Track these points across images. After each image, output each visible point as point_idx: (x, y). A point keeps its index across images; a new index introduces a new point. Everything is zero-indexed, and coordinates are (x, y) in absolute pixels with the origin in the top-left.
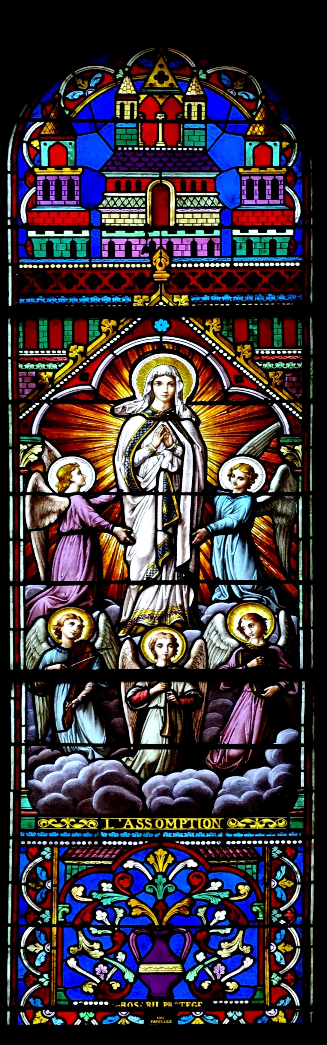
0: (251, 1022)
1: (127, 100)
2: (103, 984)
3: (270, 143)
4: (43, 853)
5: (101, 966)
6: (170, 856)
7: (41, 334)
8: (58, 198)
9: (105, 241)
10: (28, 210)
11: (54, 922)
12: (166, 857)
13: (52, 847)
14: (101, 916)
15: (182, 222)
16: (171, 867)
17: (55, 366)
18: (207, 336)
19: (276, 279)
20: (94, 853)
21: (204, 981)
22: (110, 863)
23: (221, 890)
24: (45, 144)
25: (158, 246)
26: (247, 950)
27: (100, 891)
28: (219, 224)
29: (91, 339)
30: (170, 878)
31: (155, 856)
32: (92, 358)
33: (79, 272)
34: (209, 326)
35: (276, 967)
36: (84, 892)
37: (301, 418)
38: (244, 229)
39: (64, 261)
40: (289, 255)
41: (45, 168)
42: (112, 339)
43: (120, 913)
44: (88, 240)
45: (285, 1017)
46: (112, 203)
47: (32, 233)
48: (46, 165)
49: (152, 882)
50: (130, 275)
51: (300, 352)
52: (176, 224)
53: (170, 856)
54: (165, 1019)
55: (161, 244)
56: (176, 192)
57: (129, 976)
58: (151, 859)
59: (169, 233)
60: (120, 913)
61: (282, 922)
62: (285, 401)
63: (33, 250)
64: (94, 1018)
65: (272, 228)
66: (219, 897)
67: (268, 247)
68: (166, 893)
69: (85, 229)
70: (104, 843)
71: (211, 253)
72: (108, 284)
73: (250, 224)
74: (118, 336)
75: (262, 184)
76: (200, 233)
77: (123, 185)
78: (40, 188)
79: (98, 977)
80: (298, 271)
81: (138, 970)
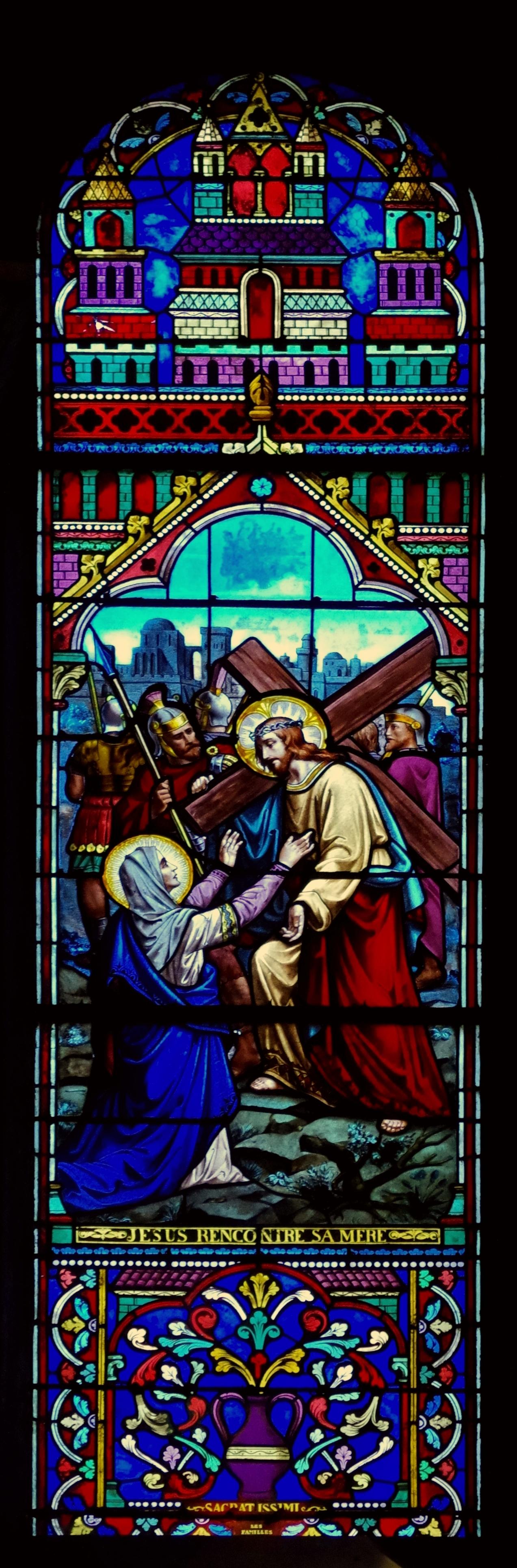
0: (390, 1534)
1: (309, 151)
2: (341, 1476)
3: (422, 214)
4: (83, 1278)
5: (170, 1448)
6: (274, 1283)
7: (437, 500)
8: (411, 295)
9: (179, 361)
10: (66, 311)
11: (101, 1382)
12: (267, 1285)
13: (97, 1269)
14: (169, 1373)
15: (295, 333)
16: (274, 1301)
17: (105, 546)
18: (328, 503)
19: (431, 419)
20: (140, 1278)
21: (321, 1473)
22: (181, 1294)
23: (348, 1336)
24: (90, 214)
25: (256, 369)
26: (384, 1426)
27: (169, 1335)
28: (348, 336)
29: (159, 506)
30: (273, 1317)
31: (251, 1284)
32: (160, 535)
33: (306, 406)
34: (332, 490)
35: (427, 1452)
36: (146, 1337)
37: (466, 629)
38: (384, 345)
39: (117, 390)
40: (449, 384)
41: (90, 249)
42: (189, 506)
43: (199, 1368)
44: (153, 358)
45: (440, 1526)
46: (189, 303)
47: (71, 348)
48: (394, 246)
49: (247, 1323)
50: (451, 413)
51: (464, 531)
52: (283, 336)
53: (274, 1283)
54: (264, 1528)
55: (261, 366)
56: (283, 286)
57: (213, 1464)
58: (244, 1289)
59: (407, 349)
60: (199, 1368)
61: (436, 1384)
62: (448, 606)
63: (74, 373)
64: (377, 1527)
65: (424, 342)
66: (371, 1378)
67: (409, 372)
68: (268, 1339)
69: (150, 342)
70: (175, 1264)
71: (334, 381)
72: (348, 427)
73: (423, 337)
74: (200, 502)
75: (111, 274)
76: (323, 350)
77: (318, 277)
78: (84, 279)
79: (166, 1464)
80: (463, 409)
81: (225, 1455)
